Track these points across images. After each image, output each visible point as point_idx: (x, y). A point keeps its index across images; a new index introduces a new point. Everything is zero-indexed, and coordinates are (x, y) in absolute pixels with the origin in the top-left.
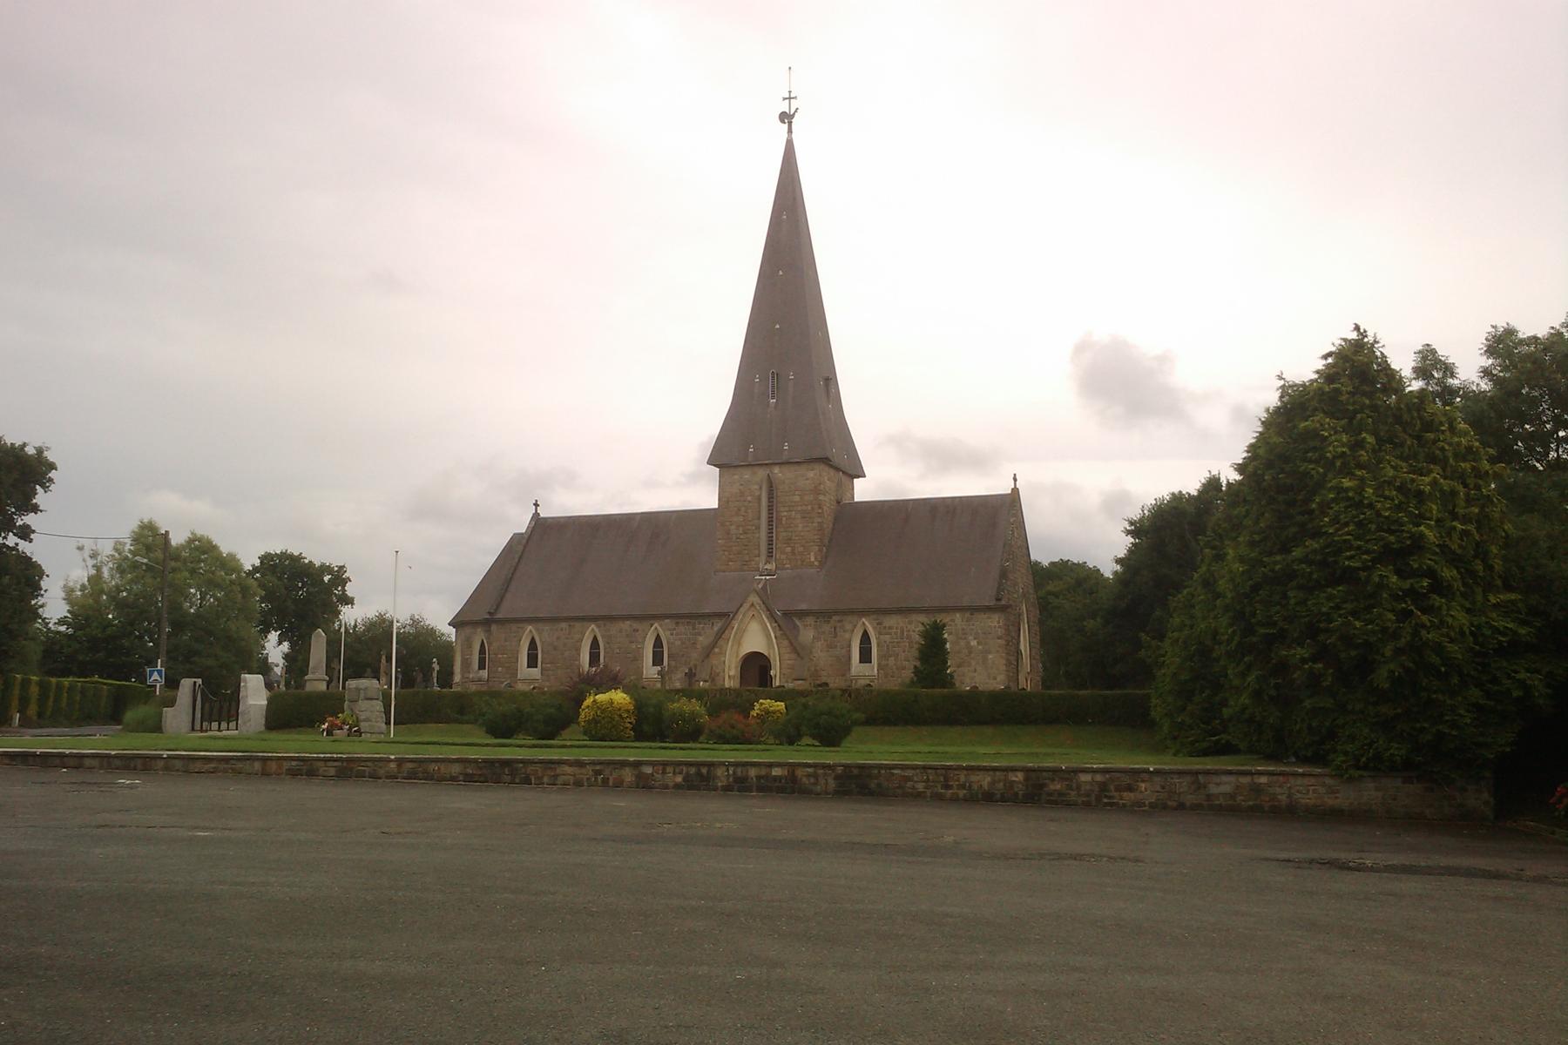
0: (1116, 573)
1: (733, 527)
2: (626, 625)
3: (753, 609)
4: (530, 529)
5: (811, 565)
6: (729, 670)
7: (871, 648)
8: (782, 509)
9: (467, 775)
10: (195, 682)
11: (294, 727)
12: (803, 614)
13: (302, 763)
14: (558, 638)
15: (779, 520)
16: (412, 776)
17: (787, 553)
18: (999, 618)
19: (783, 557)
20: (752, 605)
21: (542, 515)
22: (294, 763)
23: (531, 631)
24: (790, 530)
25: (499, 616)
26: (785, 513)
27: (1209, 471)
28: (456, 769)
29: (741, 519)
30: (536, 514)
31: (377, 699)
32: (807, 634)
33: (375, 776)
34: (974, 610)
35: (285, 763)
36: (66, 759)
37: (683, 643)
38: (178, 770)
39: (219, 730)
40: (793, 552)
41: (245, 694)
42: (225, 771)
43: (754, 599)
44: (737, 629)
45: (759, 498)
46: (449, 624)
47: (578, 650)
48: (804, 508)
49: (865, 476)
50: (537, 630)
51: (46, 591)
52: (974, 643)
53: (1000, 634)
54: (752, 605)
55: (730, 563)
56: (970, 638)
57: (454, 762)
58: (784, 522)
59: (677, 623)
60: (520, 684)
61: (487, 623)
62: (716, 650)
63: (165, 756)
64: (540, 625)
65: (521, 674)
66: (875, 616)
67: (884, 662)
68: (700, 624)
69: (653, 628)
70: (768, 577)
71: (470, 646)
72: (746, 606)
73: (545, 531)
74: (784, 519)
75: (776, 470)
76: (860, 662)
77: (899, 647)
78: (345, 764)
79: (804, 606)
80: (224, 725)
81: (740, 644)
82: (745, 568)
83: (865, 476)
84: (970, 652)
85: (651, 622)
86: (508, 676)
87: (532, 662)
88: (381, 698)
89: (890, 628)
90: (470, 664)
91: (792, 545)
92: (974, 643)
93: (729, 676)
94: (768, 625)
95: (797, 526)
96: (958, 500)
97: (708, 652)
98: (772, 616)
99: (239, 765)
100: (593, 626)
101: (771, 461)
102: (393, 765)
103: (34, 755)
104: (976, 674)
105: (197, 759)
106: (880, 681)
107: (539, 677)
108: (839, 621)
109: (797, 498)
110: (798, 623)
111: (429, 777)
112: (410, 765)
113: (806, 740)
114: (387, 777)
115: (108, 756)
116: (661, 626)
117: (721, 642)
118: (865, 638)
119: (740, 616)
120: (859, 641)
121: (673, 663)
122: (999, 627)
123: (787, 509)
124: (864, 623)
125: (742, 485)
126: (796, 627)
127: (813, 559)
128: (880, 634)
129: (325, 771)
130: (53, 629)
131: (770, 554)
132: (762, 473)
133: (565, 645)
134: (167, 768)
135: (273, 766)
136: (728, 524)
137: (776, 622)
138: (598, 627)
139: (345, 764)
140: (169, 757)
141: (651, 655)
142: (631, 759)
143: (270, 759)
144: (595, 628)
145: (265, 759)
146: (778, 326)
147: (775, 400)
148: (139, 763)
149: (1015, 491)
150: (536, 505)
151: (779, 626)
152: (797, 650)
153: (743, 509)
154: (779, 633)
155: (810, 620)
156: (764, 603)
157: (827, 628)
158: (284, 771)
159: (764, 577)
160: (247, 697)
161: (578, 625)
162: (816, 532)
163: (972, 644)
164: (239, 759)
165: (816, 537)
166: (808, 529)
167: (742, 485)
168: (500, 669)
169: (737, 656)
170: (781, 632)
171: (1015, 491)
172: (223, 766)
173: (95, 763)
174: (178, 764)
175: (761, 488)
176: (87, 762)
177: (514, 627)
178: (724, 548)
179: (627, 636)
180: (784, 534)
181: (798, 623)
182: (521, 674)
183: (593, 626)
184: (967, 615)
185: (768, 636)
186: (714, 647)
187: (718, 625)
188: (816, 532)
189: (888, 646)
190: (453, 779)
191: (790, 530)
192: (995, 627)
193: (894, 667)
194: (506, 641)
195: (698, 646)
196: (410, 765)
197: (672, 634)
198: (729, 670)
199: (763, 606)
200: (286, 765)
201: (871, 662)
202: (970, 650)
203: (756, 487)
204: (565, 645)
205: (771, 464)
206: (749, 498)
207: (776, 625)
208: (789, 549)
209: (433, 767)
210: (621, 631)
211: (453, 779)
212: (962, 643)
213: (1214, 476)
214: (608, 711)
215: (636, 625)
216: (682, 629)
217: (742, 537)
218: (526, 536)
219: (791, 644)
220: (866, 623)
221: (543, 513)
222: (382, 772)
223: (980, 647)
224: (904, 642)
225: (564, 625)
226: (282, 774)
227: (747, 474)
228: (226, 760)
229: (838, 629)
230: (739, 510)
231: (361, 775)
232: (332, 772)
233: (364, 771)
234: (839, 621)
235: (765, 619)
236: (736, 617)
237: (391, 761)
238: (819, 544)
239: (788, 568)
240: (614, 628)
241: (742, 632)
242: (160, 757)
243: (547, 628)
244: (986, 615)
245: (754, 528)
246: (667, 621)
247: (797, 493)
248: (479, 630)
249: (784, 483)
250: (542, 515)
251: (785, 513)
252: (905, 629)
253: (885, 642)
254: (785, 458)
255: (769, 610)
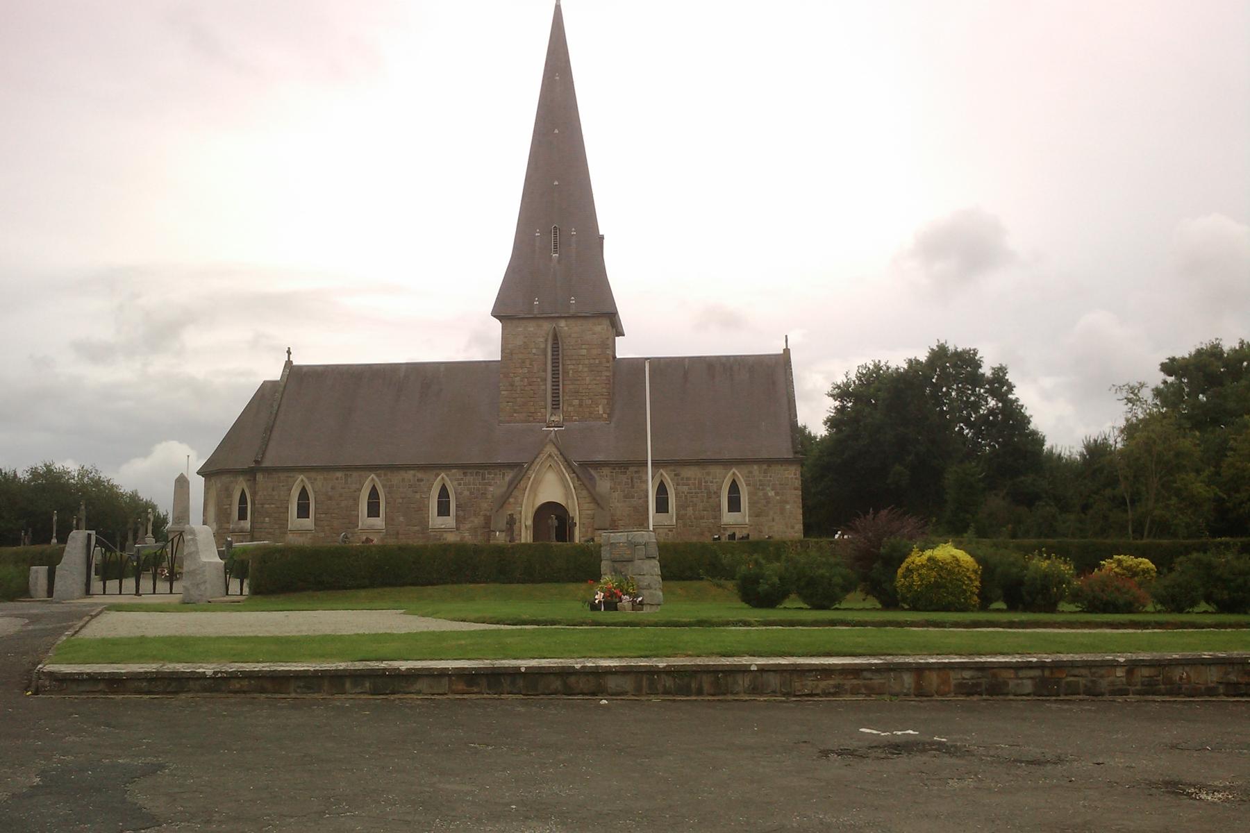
0: (826, 436)
1: (518, 378)
2: (409, 475)
3: (550, 459)
4: (286, 377)
5: (599, 418)
6: (526, 519)
7: (668, 498)
8: (569, 362)
9: (1228, 684)
10: (89, 535)
11: (303, 589)
12: (598, 465)
13: (980, 674)
14: (333, 488)
15: (566, 372)
16: (1150, 688)
17: (574, 406)
18: (796, 470)
19: (570, 409)
20: (550, 455)
21: (294, 363)
22: (967, 674)
23: (302, 480)
24: (579, 382)
25: (266, 464)
26: (572, 367)
27: (938, 340)
28: (1213, 676)
29: (526, 370)
30: (289, 363)
31: (654, 558)
32: (604, 485)
33: (1093, 692)
34: (770, 462)
35: (952, 674)
36: (572, 679)
37: (471, 493)
38: (774, 692)
39: (137, 593)
40: (580, 405)
41: (193, 549)
42: (855, 691)
43: (550, 449)
44: (534, 480)
45: (545, 349)
46: (198, 473)
47: (356, 500)
48: (592, 361)
49: (624, 335)
50: (309, 479)
51: (1202, 343)
52: (772, 494)
53: (796, 485)
54: (550, 455)
55: (515, 415)
56: (768, 489)
57: (1210, 665)
58: (570, 375)
59: (465, 474)
60: (290, 536)
61: (251, 473)
62: (511, 500)
63: (754, 668)
64: (313, 475)
65: (292, 524)
66: (673, 468)
67: (683, 512)
68: (489, 473)
69: (440, 477)
70: (556, 429)
71: (230, 496)
72: (543, 456)
73: (296, 376)
74: (571, 372)
75: (562, 323)
76: (657, 512)
77: (697, 497)
78: (1047, 673)
79: (600, 457)
80: (146, 584)
81: (536, 495)
82: (531, 419)
83: (624, 335)
84: (768, 503)
85: (438, 471)
86: (276, 526)
87: (303, 511)
88: (658, 558)
89: (688, 479)
90: (230, 514)
91: (580, 398)
92: (772, 494)
93: (526, 526)
94: (567, 475)
95: (585, 380)
96: (732, 359)
97: (503, 501)
98: (569, 465)
99: (877, 680)
100: (373, 475)
101: (557, 315)
102: (1120, 673)
103: (514, 673)
104: (774, 524)
105: (810, 671)
106: (679, 530)
107: (313, 527)
108: (636, 472)
109: (584, 352)
110: (592, 472)
111: (1174, 690)
112: (1146, 672)
113: (793, 596)
114: (1113, 693)
115: (652, 672)
116: (447, 475)
117: (516, 493)
118: (734, 488)
119: (536, 467)
120: (437, 496)
121: (461, 513)
122: (796, 479)
123: (574, 362)
124: (662, 474)
125: (526, 337)
126: (592, 478)
127: (601, 412)
128: (678, 485)
129: (1018, 685)
130: (545, 449)
131: (556, 405)
132: (547, 326)
133: (341, 495)
134: (755, 690)
135: (933, 679)
136: (512, 375)
137: (574, 472)
138: (378, 476)
139: (1047, 673)
140: (763, 670)
141: (437, 503)
142: (869, 627)
143: (929, 667)
144: (375, 477)
145: (919, 670)
146: (556, 183)
147: (557, 255)
148: (706, 681)
149: (787, 351)
150: (289, 353)
151: (578, 476)
152: (596, 500)
153: (528, 362)
154: (577, 483)
155: (606, 471)
156: (561, 454)
157: (623, 478)
158: (952, 689)
159: (552, 429)
160: (197, 552)
161: (355, 474)
162: (604, 385)
163: (770, 494)
164: (878, 669)
165: (604, 390)
166: (595, 382)
167: (526, 337)
168: (267, 519)
169: (533, 507)
170: (580, 483)
171: (787, 351)
172: (851, 682)
173: (628, 683)
174: (774, 681)
175: (546, 341)
176: (612, 683)
177: (283, 476)
178: (508, 400)
179: (411, 486)
180: (571, 387)
181: (592, 472)
182: (292, 524)
183: (373, 475)
184: (765, 467)
185: (566, 487)
186: (508, 498)
187: (509, 475)
188: (604, 385)
189: (686, 496)
190: (1211, 691)
191: (579, 382)
192: (792, 478)
193: (693, 516)
194: (273, 490)
195: (490, 496)
196: (1146, 672)
197: (460, 484)
198: (526, 519)
199: (560, 456)
200: (955, 677)
201: (668, 512)
202: (768, 500)
203: (542, 340)
204: (341, 495)
205: (558, 317)
206: (534, 351)
207: (574, 475)
208: (576, 402)
209: (1178, 674)
210: (403, 480)
211: (1211, 691)
212: (761, 494)
213: (942, 344)
214: (946, 573)
215: (420, 475)
216: (469, 478)
217: (526, 389)
218: (283, 384)
219: (590, 493)
220: (665, 474)
221: (297, 361)
222: (1104, 684)
223: (778, 498)
224: (702, 492)
225: (339, 474)
226: (949, 693)
227: (531, 327)
228: (856, 671)
229: (635, 480)
230: (524, 362)
231: (1073, 690)
232: (1028, 686)
233: (1078, 682)
234: (636, 472)
235: (564, 469)
236: (533, 467)
237: (1118, 665)
238: (607, 397)
239: (575, 420)
240: (396, 478)
241: (537, 482)
242: (744, 670)
243: (320, 477)
244: (784, 467)
245: (539, 380)
246: (453, 471)
247: (583, 347)
248: (241, 479)
249: (570, 336)
250: (294, 363)
251: (572, 367)
252: (703, 481)
253: (683, 492)
254: (572, 312)
255: (566, 461)
